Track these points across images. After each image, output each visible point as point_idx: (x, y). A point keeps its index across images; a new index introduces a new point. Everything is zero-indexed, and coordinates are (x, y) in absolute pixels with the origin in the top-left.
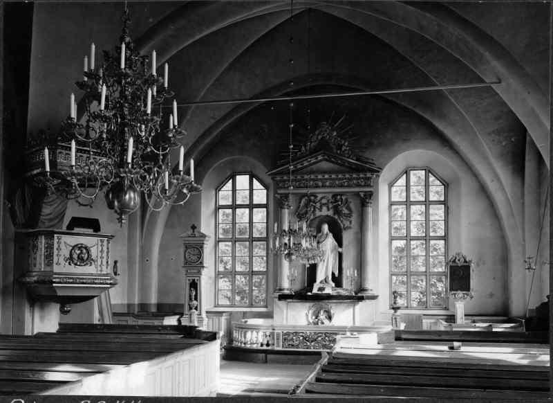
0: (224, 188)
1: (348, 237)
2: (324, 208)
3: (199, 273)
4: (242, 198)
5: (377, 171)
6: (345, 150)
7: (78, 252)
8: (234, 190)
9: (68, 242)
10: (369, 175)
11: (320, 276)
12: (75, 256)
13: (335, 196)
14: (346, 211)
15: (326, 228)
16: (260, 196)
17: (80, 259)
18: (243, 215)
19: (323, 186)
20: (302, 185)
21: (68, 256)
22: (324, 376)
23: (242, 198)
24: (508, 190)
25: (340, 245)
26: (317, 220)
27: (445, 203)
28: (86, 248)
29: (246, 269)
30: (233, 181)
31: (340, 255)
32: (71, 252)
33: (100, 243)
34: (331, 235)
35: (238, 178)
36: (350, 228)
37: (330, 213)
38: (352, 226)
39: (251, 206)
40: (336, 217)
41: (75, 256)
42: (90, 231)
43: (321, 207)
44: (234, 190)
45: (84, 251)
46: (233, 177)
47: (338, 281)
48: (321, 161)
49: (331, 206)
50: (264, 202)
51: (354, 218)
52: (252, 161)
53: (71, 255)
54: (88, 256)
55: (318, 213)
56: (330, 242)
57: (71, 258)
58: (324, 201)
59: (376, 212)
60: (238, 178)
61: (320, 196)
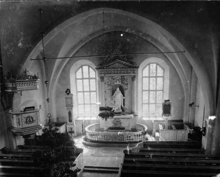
1: (126, 92)
2: (118, 82)
3: (72, 109)
4: (86, 75)
5: (138, 67)
6: (125, 59)
7: (29, 119)
8: (82, 72)
9: (24, 116)
10: (135, 69)
13: (122, 76)
15: (118, 89)
16: (160, 72)
17: (30, 121)
18: (86, 82)
19: (117, 73)
20: (109, 73)
22: (85, 169)
23: (86, 75)
26: (115, 86)
27: (163, 77)
29: (75, 151)
30: (82, 68)
31: (124, 100)
32: (26, 120)
34: (120, 92)
36: (127, 89)
37: (120, 83)
38: (128, 88)
39: (89, 78)
40: (122, 85)
41: (28, 121)
43: (116, 81)
44: (82, 72)
45: (31, 118)
46: (82, 67)
48: (116, 63)
49: (120, 80)
50: (94, 77)
53: (26, 121)
54: (33, 120)
55: (115, 83)
56: (120, 94)
57: (27, 122)
58: (118, 78)
59: (137, 83)
61: (116, 77)
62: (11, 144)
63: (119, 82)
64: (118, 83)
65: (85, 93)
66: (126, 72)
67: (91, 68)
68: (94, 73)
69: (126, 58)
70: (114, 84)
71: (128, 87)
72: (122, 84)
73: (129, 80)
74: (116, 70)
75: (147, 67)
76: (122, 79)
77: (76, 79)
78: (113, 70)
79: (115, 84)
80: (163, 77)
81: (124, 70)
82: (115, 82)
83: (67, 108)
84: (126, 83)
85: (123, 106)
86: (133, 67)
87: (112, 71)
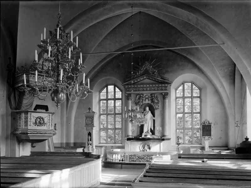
0: (103, 91)
1: (157, 113)
2: (147, 100)
3: (92, 129)
5: (170, 83)
6: (156, 74)
7: (39, 120)
8: (107, 92)
10: (166, 85)
11: (145, 130)
12: (38, 122)
13: (151, 94)
14: (156, 101)
15: (147, 108)
16: (119, 95)
17: (40, 123)
19: (147, 90)
21: (34, 122)
24: (228, 93)
25: (154, 116)
26: (144, 105)
28: (42, 118)
31: (154, 121)
33: (48, 116)
34: (150, 112)
35: (109, 86)
36: (158, 109)
37: (150, 102)
39: (115, 99)
40: (152, 104)
41: (38, 122)
42: (44, 111)
44: (107, 92)
45: (42, 120)
46: (107, 86)
47: (153, 132)
48: (145, 79)
49: (150, 99)
50: (121, 97)
51: (160, 104)
52: (114, 79)
53: (36, 121)
55: (144, 102)
56: (149, 115)
57: (36, 123)
58: (147, 97)
59: (170, 102)
60: (109, 86)
61: (145, 95)
62: (14, 151)
63: (149, 100)
64: (147, 102)
65: (109, 102)
66: (156, 89)
67: (118, 87)
68: (121, 93)
69: (157, 73)
70: (143, 103)
71: (158, 107)
72: (151, 102)
73: (160, 98)
74: (145, 86)
75: (116, 89)
76: (152, 97)
77: (100, 100)
78: (142, 86)
79: (144, 103)
80: (200, 97)
81: (154, 87)
82: (144, 101)
83: (87, 128)
84: (156, 101)
85: (152, 129)
86: (165, 83)
87: (141, 87)
